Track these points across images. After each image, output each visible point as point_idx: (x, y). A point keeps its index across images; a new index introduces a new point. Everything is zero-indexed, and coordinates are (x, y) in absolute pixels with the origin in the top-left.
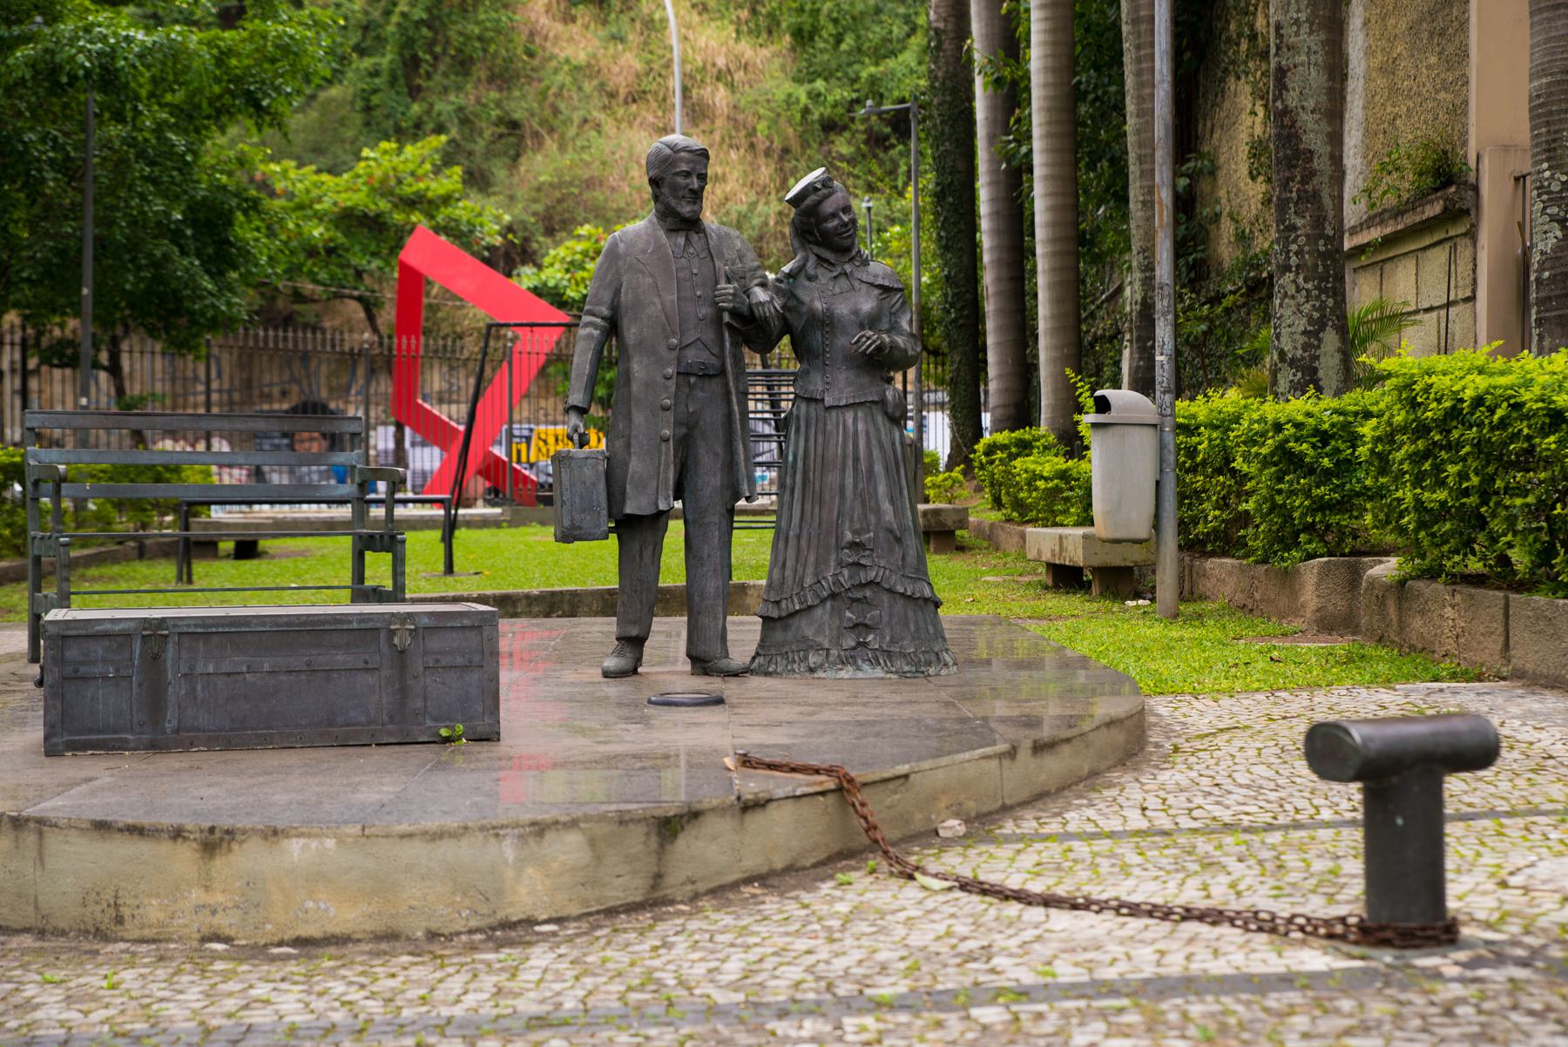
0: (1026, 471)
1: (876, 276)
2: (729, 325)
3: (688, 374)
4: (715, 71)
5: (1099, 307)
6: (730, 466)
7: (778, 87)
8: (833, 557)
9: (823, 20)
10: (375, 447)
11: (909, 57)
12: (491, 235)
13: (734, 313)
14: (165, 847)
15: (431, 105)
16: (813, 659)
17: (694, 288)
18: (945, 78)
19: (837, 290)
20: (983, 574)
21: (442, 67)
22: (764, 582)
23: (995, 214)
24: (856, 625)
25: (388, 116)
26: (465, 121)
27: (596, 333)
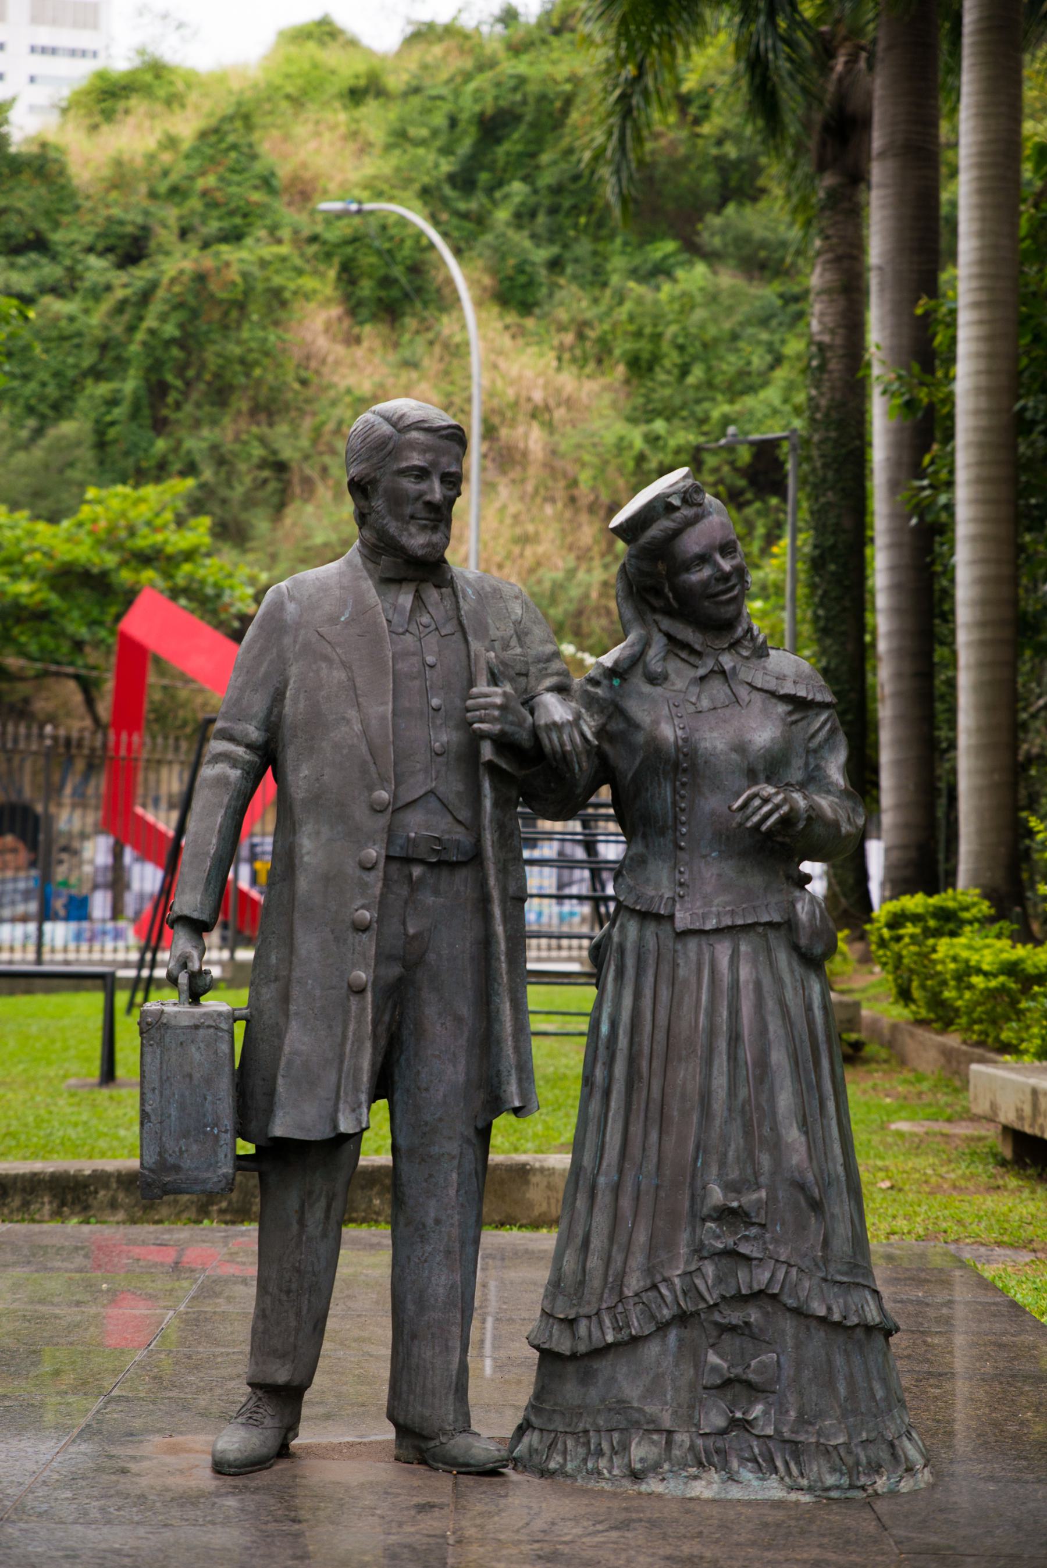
0: (955, 959)
1: (781, 678)
2: (491, 766)
3: (408, 861)
4: (529, 407)
5: (1034, 716)
6: (485, 1043)
7: (607, 427)
8: (684, 1236)
9: (665, 346)
10: (92, 862)
11: (772, 394)
13: (503, 743)
15: (179, 443)
16: (640, 1451)
17: (426, 693)
18: (829, 408)
19: (705, 703)
20: (890, 1112)
21: (195, 396)
22: (562, 1161)
23: (896, 588)
24: (728, 1383)
25: (127, 454)
26: (221, 461)
27: (235, 774)
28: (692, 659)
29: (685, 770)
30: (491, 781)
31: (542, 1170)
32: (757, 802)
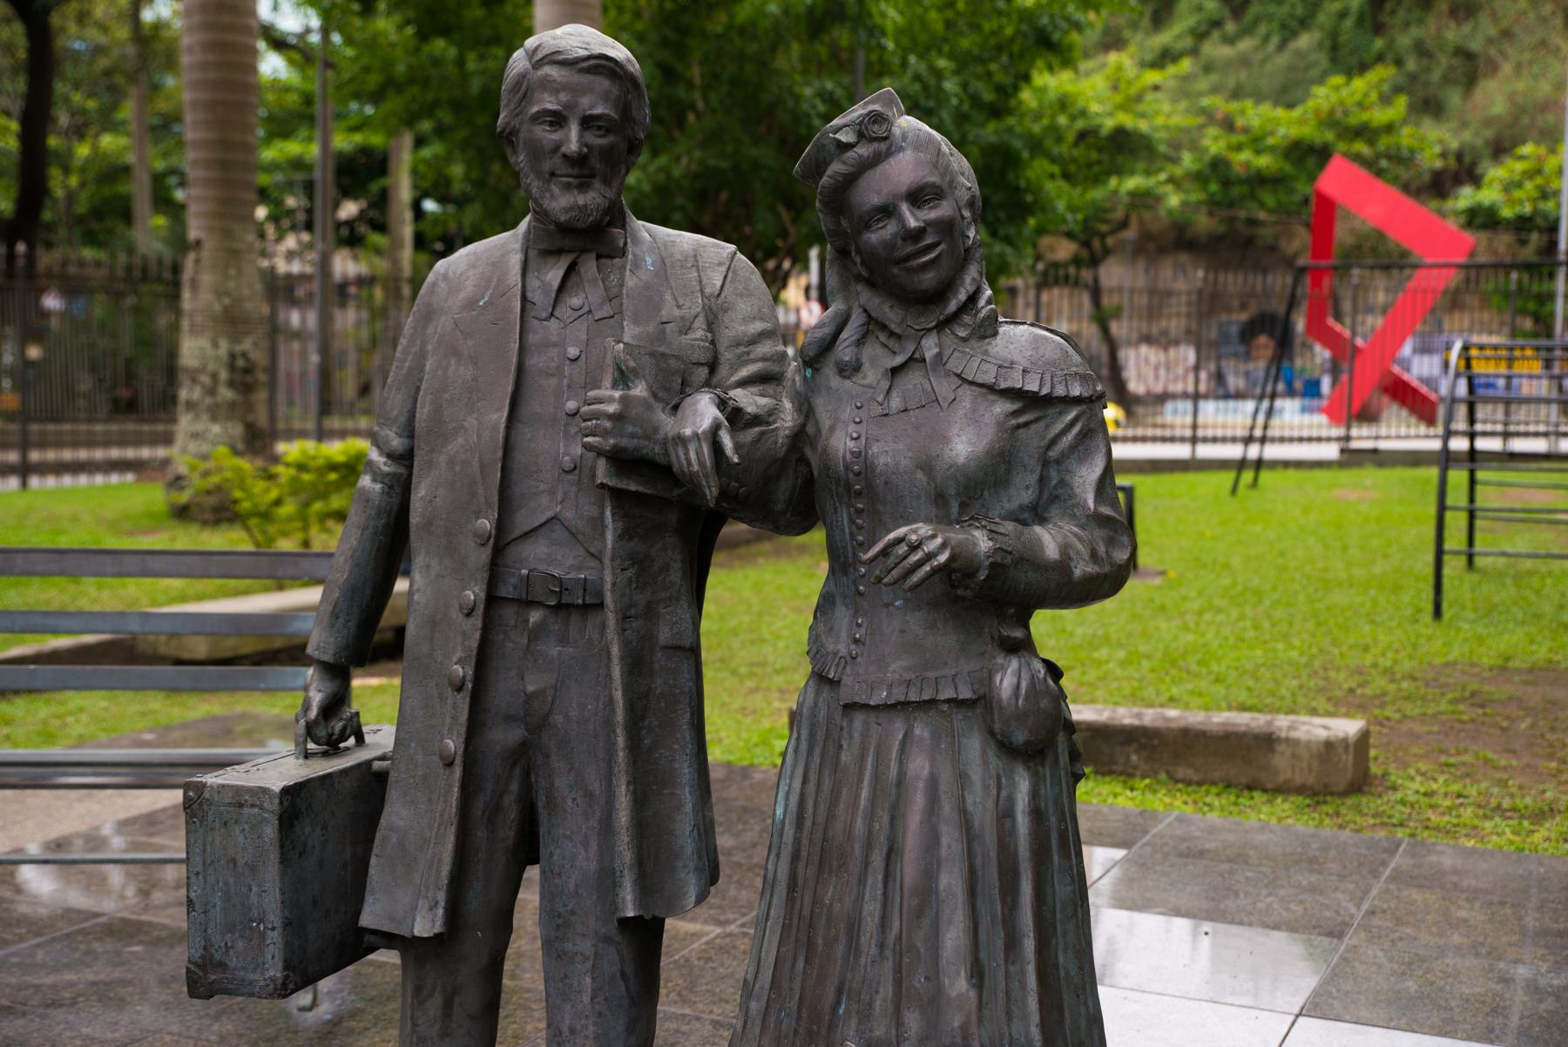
1: (1006, 366)
12: (1430, 160)
19: (896, 403)
28: (892, 343)
29: (859, 494)
30: (613, 507)
31: (1287, 740)
32: (902, 549)
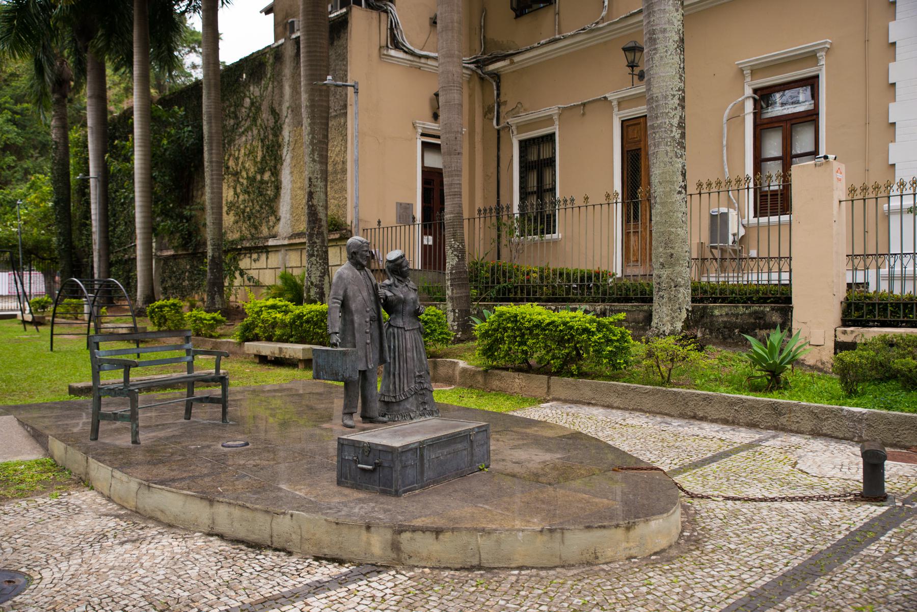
14: (613, 531)
